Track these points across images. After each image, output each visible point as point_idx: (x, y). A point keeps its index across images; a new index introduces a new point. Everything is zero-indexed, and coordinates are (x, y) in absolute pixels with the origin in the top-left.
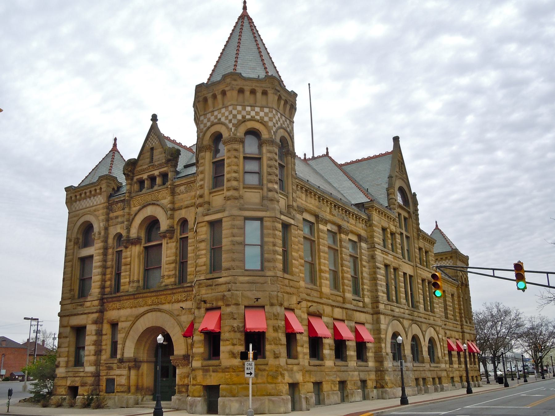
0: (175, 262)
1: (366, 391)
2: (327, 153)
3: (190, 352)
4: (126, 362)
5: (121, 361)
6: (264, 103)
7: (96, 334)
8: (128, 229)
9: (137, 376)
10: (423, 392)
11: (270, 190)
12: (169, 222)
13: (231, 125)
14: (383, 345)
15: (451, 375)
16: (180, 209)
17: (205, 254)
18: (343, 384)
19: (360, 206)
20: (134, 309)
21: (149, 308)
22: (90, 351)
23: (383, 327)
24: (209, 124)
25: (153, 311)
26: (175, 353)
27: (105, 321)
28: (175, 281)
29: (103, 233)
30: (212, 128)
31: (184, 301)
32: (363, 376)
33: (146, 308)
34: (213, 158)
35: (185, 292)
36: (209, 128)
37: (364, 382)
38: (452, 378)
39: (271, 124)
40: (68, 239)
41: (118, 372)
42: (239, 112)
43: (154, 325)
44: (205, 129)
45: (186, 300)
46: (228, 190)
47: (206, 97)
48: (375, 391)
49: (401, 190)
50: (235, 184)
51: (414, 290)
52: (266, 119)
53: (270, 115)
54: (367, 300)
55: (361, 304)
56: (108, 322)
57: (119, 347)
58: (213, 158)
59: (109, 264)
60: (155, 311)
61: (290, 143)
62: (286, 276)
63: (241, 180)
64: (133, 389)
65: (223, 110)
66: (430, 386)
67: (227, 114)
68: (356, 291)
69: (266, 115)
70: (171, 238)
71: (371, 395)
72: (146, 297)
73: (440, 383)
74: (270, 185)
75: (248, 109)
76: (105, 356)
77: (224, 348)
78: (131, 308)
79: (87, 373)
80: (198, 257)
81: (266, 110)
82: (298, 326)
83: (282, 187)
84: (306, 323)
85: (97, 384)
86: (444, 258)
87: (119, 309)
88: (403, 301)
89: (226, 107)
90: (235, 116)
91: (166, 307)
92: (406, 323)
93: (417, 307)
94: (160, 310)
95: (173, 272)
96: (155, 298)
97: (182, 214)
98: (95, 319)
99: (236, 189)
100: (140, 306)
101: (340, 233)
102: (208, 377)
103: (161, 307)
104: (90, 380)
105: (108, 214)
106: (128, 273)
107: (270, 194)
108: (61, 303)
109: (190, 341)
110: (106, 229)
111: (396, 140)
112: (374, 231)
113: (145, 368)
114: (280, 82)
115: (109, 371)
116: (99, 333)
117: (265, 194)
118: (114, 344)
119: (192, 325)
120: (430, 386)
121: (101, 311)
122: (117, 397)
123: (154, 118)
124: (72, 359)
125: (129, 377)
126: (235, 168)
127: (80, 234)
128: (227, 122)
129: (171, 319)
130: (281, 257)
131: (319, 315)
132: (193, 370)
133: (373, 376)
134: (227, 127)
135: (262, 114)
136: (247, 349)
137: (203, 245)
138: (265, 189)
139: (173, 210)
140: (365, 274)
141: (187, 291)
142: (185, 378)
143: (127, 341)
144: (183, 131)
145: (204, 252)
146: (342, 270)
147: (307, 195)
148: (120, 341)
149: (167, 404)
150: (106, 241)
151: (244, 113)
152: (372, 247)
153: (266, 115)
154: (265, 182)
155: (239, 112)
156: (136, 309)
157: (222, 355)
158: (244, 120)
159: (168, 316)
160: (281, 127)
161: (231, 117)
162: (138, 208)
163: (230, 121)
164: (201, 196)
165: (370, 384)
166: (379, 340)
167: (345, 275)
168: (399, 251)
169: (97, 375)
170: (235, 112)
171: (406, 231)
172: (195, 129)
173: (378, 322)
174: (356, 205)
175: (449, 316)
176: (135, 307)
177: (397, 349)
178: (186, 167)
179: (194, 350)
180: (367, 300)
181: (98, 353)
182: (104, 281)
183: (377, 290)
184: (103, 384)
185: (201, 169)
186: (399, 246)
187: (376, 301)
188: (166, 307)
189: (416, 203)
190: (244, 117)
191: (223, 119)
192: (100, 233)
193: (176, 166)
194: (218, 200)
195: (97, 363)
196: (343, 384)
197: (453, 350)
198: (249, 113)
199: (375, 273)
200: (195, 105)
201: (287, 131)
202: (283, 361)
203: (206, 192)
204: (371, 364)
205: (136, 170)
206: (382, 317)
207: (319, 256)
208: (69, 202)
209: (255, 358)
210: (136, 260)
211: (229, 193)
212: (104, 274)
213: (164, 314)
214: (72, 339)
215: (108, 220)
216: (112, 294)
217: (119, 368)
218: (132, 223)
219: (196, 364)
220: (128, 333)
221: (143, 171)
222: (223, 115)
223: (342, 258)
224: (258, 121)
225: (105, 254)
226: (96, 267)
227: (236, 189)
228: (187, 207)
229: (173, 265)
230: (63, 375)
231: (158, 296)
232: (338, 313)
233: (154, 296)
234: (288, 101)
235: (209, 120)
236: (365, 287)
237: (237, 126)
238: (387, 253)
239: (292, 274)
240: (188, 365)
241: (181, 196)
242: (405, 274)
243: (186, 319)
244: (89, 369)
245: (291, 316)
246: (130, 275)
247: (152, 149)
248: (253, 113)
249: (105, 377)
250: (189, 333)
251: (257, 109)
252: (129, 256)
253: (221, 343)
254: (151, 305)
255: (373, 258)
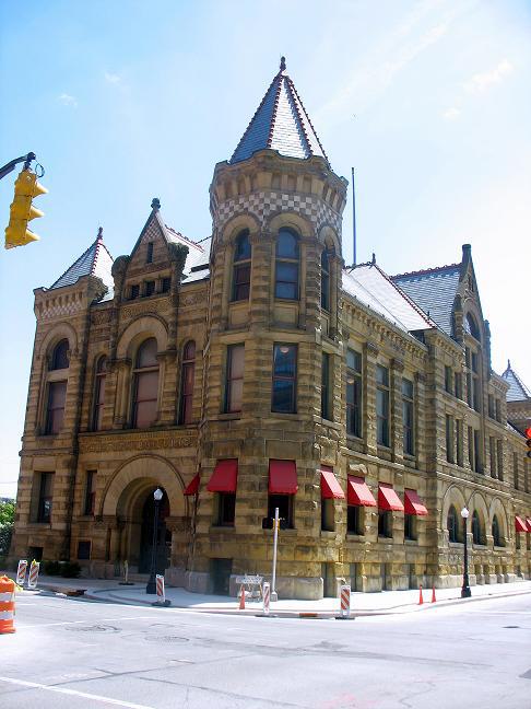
0: (176, 393)
1: (413, 577)
2: (374, 260)
3: (192, 514)
5: (100, 518)
6: (306, 190)
8: (115, 345)
9: (120, 539)
10: (483, 582)
11: (308, 306)
12: (169, 341)
13: (261, 218)
14: (438, 519)
15: (517, 563)
16: (186, 323)
17: (219, 386)
18: (386, 567)
19: (419, 334)
22: (58, 503)
23: (439, 494)
24: (231, 214)
26: (172, 513)
27: (80, 466)
28: (175, 420)
29: (81, 349)
30: (236, 220)
32: (411, 559)
34: (236, 260)
36: (231, 219)
37: (412, 567)
38: (519, 567)
39: (314, 219)
40: (36, 357)
41: (95, 532)
42: (273, 201)
44: (226, 221)
46: (254, 301)
47: (230, 181)
48: (424, 578)
49: (469, 316)
50: (264, 295)
51: (479, 448)
52: (308, 212)
53: (313, 207)
54: (421, 458)
55: (413, 464)
57: (98, 500)
58: (236, 260)
59: (87, 391)
61: (336, 245)
62: (326, 422)
63: (272, 290)
65: (252, 198)
66: (493, 575)
67: (227, 210)
68: (409, 449)
69: (309, 206)
70: (173, 362)
71: (419, 583)
73: (486, 572)
74: (310, 300)
75: (285, 197)
76: (77, 511)
77: (241, 510)
79: (55, 530)
80: (207, 389)
81: (309, 200)
82: (337, 488)
83: (324, 306)
84: (376, 491)
85: (67, 544)
86: (517, 409)
88: (466, 464)
89: (257, 195)
90: (267, 206)
91: (162, 452)
92: (468, 493)
93: (482, 472)
94: (152, 456)
95: (173, 408)
97: (187, 331)
99: (264, 301)
100: (127, 449)
101: (392, 369)
102: (217, 547)
103: (154, 452)
104: (60, 539)
105: (88, 326)
106: (111, 406)
107: (310, 312)
108: (23, 439)
109: (192, 499)
110: (86, 345)
111: (467, 248)
112: (434, 367)
113: (130, 528)
114: (328, 166)
116: (72, 480)
117: (303, 311)
118: (90, 497)
119: (197, 478)
120: (493, 575)
121: (76, 451)
123: (156, 204)
124: (35, 512)
125: (109, 540)
126: (265, 273)
127: (51, 355)
128: (256, 213)
130: (320, 397)
131: (360, 478)
132: (198, 536)
133: (422, 559)
134: (257, 220)
135: (303, 205)
136: (272, 514)
137: (217, 373)
138: (303, 305)
139: (176, 324)
140: (420, 425)
142: (183, 546)
144: (193, 226)
145: (218, 383)
146: (393, 418)
147: (353, 318)
148: (98, 495)
150: (84, 361)
151: (279, 203)
152: (432, 387)
153: (309, 206)
154: (303, 296)
155: (273, 201)
157: (237, 521)
158: (279, 211)
159: (164, 465)
160: (326, 224)
161: (262, 207)
162: (129, 319)
163: (261, 212)
164: (218, 308)
165: (419, 570)
166: (433, 511)
167: (396, 424)
168: (464, 396)
169: (68, 534)
170: (267, 201)
171: (474, 370)
172: (210, 220)
173: (434, 487)
174: (412, 332)
175: (519, 485)
177: (454, 521)
178: (194, 270)
179: (201, 511)
180: (421, 458)
181: (70, 505)
182: (79, 413)
183: (434, 447)
184: (75, 548)
185: (218, 272)
186: (464, 391)
187: (432, 458)
189: (487, 333)
190: (279, 207)
191: (251, 209)
192: (77, 350)
193: (182, 266)
194: (240, 312)
195: (68, 519)
196: (386, 567)
197: (522, 529)
198: (285, 203)
199: (434, 423)
200: (212, 189)
201: (333, 229)
202: (316, 531)
203: (224, 304)
204: (421, 541)
205: (129, 269)
206: (439, 483)
207: (365, 396)
208: (38, 307)
209: (282, 526)
210: (124, 388)
211: (257, 307)
212: (80, 404)
214: (328, 521)
215: (87, 333)
216: (88, 428)
217: (97, 527)
218: (119, 340)
219: (203, 528)
220: (109, 484)
221: (138, 272)
222: (252, 203)
223: (393, 401)
224: (298, 214)
225: (83, 378)
226: (70, 394)
227: (264, 301)
228: (194, 322)
229: (173, 399)
230: (23, 532)
232: (385, 475)
234: (336, 190)
235: (231, 209)
236: (420, 441)
237: (269, 218)
238: (449, 399)
239: (332, 420)
241: (189, 308)
242: (470, 428)
243: (188, 469)
244: (59, 526)
245: (328, 476)
246: (114, 408)
247: (151, 244)
248: (291, 204)
250: (193, 488)
251: (297, 198)
252: (114, 383)
253: (237, 504)
255: (432, 401)
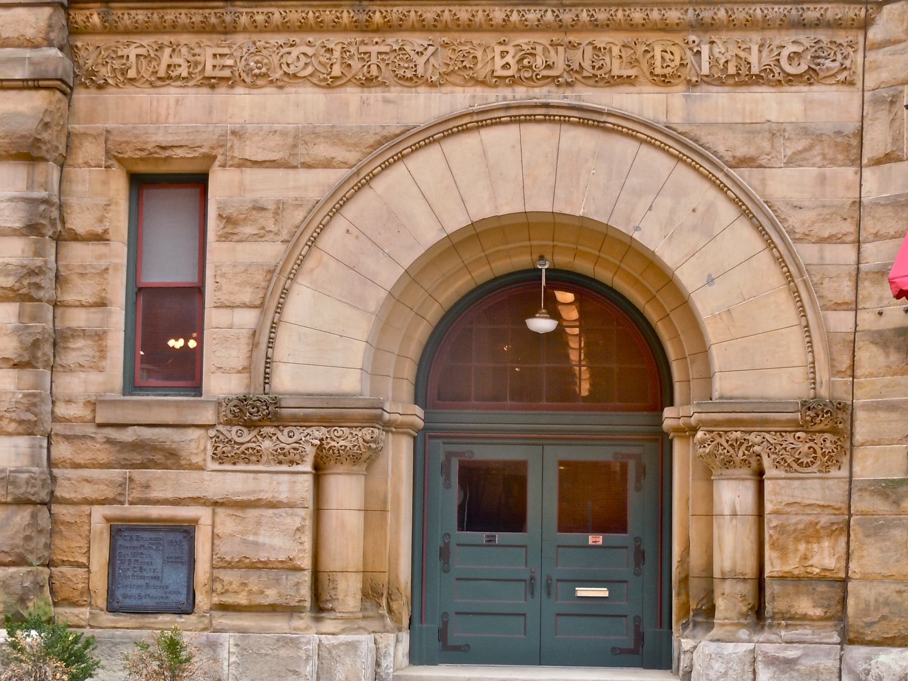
4: (304, 421)
5: (257, 412)
7: (32, 229)
20: (352, 95)
21: (493, 97)
25: (530, 120)
27: (90, 150)
31: (790, 79)
33: (460, 99)
35: (802, 25)
43: (541, 204)
45: (811, 77)
56: (114, 157)
60: (547, 120)
64: (347, 592)
72: (470, 27)
78: (331, 83)
87: (211, 83)
91: (642, 102)
94: (591, 119)
96: (543, 39)
98: (30, 126)
100: (413, 81)
115: (139, 475)
122: (228, 640)
129: (685, 175)
141: (817, 24)
143: (302, 302)
149: (113, 621)
156: (375, 95)
176: (368, 82)
188: (642, 102)
213: (624, 147)
220: (305, 240)
231: (575, 27)
233: (540, 27)
240: (831, 461)
249: (99, 513)
254: (513, 81)
